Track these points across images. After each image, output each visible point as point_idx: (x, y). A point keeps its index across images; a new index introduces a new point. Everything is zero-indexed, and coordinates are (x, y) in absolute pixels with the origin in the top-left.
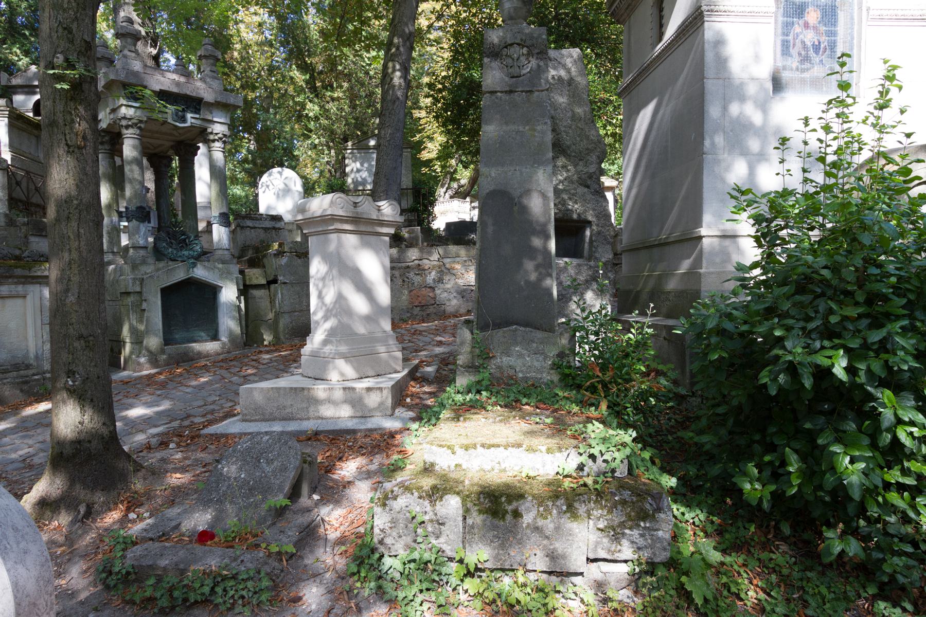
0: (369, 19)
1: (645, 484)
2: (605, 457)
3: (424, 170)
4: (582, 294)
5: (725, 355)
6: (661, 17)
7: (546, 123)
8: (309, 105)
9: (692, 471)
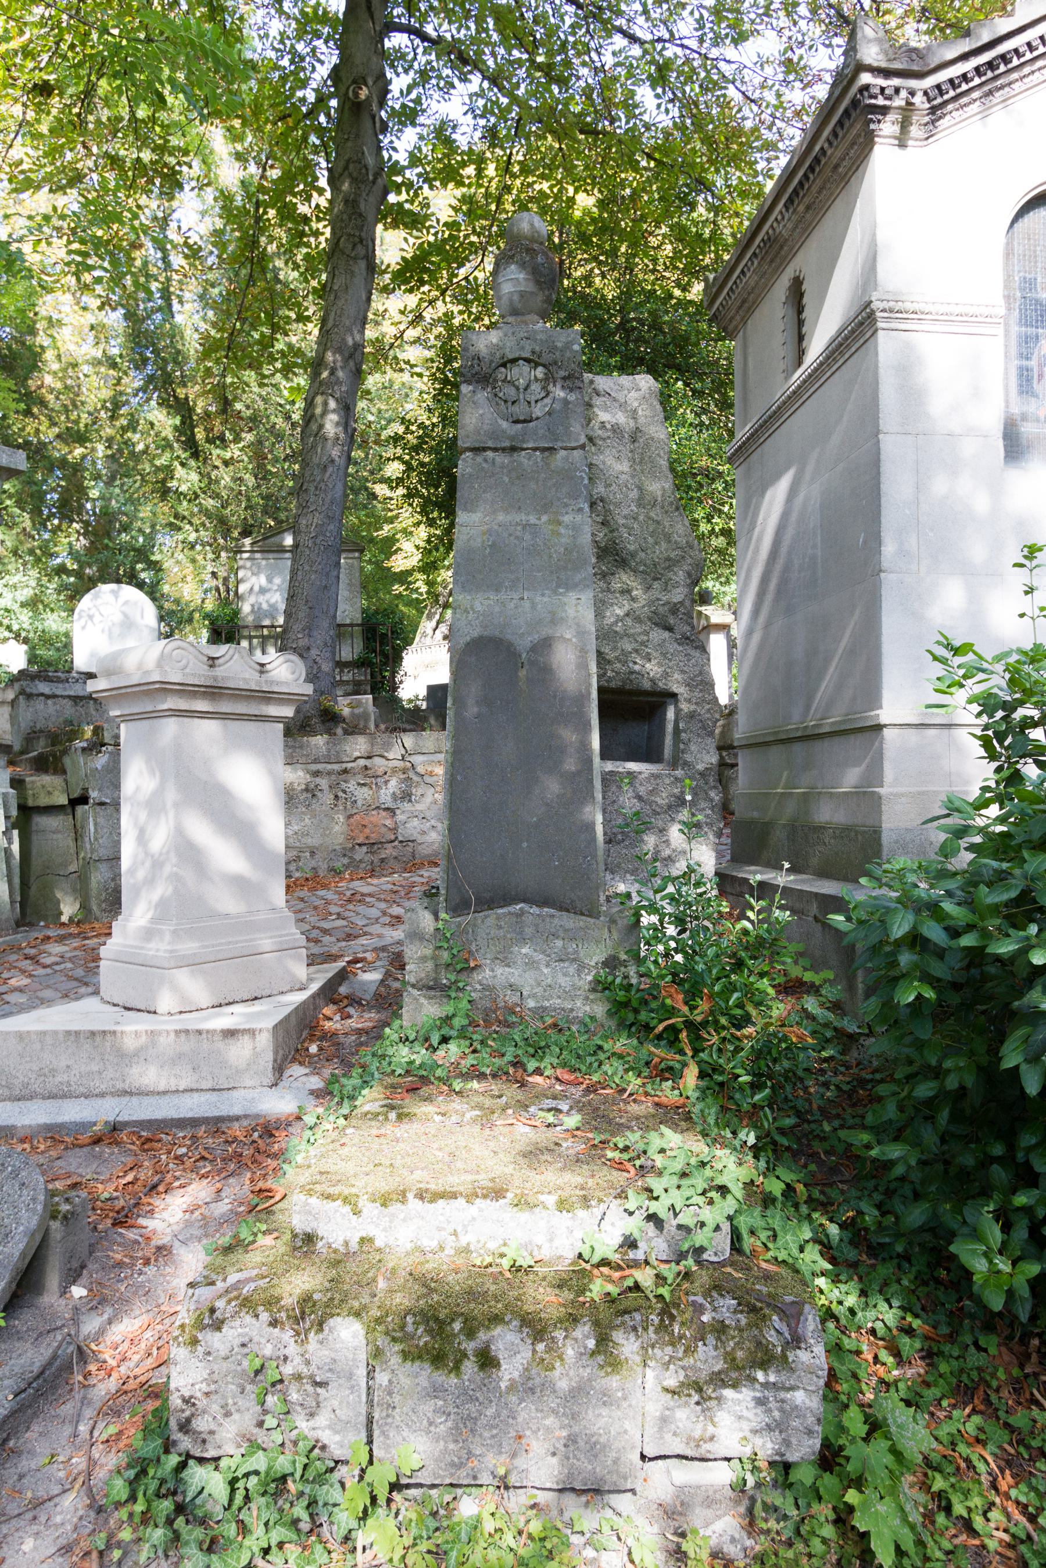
0: (288, 320)
1: (767, 1277)
2: (682, 1219)
3: (398, 589)
4: (662, 831)
5: (929, 994)
6: (801, 323)
7: (580, 510)
8: (180, 472)
9: (871, 1216)
